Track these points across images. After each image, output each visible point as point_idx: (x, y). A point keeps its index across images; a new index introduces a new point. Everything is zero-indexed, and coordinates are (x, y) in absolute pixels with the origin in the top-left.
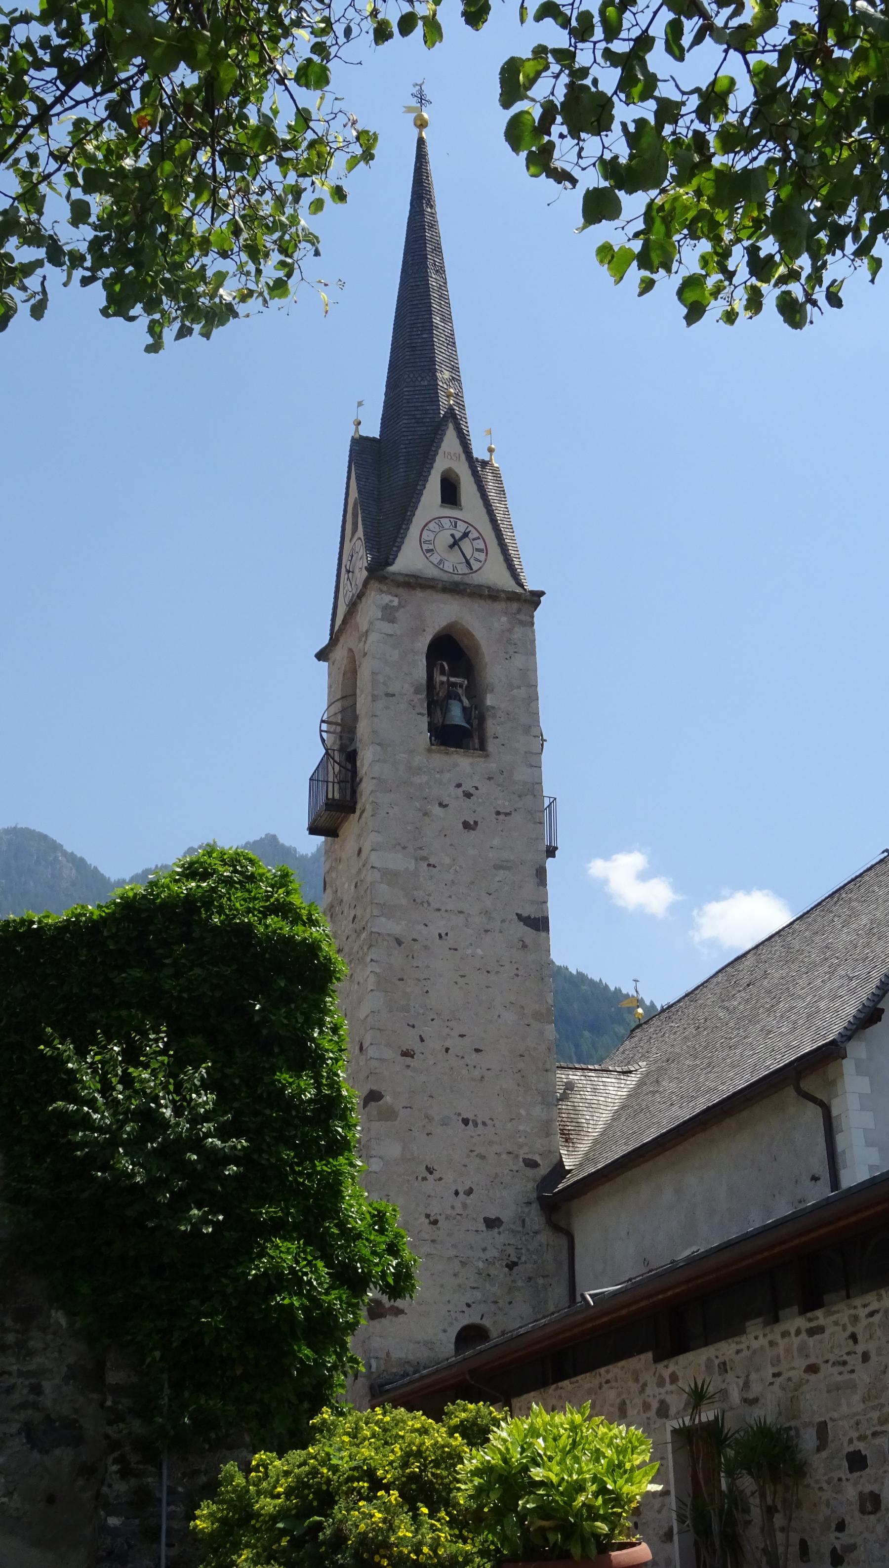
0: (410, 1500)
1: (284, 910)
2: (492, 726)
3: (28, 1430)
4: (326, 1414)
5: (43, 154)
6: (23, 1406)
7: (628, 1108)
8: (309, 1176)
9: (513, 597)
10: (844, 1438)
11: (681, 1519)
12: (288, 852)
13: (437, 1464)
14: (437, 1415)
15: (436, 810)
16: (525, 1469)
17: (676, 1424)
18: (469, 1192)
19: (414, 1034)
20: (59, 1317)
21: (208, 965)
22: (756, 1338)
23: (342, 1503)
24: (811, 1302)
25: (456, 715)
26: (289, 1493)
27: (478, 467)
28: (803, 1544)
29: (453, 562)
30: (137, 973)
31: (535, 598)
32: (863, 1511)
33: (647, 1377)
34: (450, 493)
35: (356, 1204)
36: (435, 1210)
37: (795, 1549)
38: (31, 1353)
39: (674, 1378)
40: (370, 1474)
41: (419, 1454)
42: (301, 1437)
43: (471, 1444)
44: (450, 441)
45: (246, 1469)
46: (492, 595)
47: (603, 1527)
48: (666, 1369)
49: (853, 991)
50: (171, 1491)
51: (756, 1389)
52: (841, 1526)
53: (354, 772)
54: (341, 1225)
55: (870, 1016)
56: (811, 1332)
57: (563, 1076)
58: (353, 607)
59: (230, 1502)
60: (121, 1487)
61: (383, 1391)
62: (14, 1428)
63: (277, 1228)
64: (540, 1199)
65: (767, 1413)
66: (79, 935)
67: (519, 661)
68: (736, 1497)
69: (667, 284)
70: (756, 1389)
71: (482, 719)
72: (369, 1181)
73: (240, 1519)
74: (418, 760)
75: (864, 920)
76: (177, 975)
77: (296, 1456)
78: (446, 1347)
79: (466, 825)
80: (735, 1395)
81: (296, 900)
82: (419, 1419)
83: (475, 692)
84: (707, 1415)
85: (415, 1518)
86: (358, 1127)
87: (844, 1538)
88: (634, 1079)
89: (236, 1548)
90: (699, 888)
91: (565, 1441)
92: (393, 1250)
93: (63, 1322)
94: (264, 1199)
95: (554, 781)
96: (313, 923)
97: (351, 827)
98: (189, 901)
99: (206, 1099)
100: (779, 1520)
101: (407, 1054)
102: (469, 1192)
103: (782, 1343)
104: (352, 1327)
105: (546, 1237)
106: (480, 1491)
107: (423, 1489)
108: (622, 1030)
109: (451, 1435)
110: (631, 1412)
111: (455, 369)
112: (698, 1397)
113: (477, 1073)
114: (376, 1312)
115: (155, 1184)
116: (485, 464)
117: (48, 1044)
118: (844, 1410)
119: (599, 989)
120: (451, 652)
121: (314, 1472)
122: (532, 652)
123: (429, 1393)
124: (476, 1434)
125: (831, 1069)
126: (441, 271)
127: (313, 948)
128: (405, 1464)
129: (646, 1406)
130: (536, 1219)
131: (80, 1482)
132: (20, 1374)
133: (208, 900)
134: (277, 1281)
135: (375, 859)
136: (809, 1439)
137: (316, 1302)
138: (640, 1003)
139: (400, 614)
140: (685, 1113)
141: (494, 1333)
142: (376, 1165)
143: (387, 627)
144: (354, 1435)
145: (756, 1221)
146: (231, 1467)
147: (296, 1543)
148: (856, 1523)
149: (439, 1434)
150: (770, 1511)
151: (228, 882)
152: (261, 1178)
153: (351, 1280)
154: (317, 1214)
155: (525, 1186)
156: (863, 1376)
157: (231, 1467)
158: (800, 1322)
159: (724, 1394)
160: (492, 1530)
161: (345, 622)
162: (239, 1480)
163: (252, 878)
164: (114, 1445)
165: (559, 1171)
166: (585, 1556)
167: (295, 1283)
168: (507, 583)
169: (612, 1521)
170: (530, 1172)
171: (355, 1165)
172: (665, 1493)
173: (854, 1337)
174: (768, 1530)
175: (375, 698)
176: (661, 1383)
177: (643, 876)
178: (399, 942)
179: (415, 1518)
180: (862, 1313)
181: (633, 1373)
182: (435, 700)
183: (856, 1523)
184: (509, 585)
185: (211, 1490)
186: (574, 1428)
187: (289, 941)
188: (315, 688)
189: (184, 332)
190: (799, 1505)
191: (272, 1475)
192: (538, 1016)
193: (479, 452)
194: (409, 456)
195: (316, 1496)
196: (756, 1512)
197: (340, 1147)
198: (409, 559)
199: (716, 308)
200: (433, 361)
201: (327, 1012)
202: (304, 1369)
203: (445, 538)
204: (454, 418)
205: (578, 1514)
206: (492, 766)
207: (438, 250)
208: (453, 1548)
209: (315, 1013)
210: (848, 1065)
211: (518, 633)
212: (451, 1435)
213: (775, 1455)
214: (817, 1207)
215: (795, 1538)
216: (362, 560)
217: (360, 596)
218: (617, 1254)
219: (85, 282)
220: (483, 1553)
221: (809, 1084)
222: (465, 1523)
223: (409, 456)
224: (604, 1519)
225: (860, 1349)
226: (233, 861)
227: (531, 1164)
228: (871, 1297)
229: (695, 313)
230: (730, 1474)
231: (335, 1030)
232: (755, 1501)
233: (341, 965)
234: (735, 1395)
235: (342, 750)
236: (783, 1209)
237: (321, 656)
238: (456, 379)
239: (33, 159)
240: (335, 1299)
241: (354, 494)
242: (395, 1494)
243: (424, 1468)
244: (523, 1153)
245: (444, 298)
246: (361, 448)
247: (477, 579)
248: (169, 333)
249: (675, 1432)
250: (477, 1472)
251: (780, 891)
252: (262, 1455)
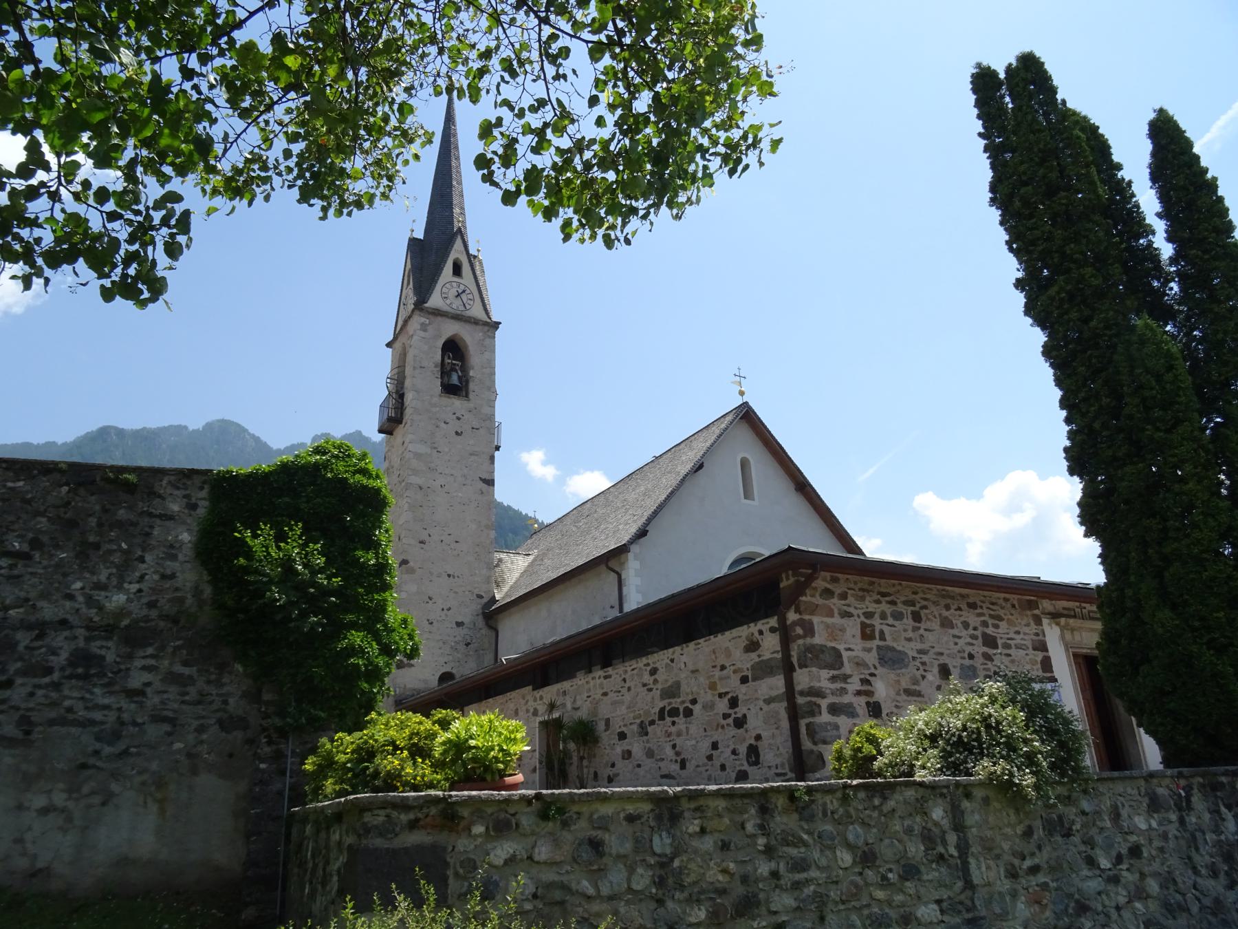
0: (413, 756)
1: (364, 472)
2: (472, 386)
3: (220, 722)
4: (373, 715)
5: (272, 121)
6: (217, 711)
7: (527, 572)
8: (371, 601)
9: (485, 324)
10: (617, 726)
11: (540, 763)
12: (367, 440)
13: (426, 738)
14: (427, 715)
15: (443, 425)
16: (467, 740)
17: (541, 719)
18: (449, 609)
19: (426, 533)
20: (239, 668)
21: (325, 498)
22: (581, 680)
23: (379, 757)
24: (606, 664)
25: (454, 379)
26: (353, 752)
27: (471, 258)
28: (596, 774)
29: (457, 304)
30: (287, 499)
31: (496, 325)
32: (623, 758)
33: (529, 697)
34: (457, 270)
35: (393, 615)
36: (431, 618)
37: (592, 776)
38: (223, 685)
39: (541, 698)
40: (393, 743)
41: (418, 734)
42: (359, 726)
43: (443, 729)
44: (458, 244)
45: (332, 741)
46: (476, 322)
47: (501, 766)
48: (538, 694)
49: (635, 521)
50: (293, 752)
51: (579, 703)
52: (613, 765)
53: (403, 404)
54: (386, 625)
55: (642, 533)
56: (606, 677)
57: (498, 556)
58: (406, 322)
59: (323, 757)
60: (267, 749)
61: (401, 704)
62: (213, 721)
63: (354, 626)
64: (483, 613)
65: (583, 714)
66: (256, 480)
67: (487, 355)
68: (566, 752)
69: (557, 222)
70: (579, 703)
71: (467, 382)
72: (399, 603)
73: (328, 764)
74: (435, 400)
75: (642, 488)
76: (308, 502)
77: (357, 734)
78: (433, 682)
79: (457, 433)
80: (569, 706)
81: (370, 467)
82: (419, 717)
83: (465, 369)
84: (556, 715)
85: (415, 763)
86: (395, 578)
87: (615, 770)
88: (531, 558)
89: (326, 778)
90: (568, 466)
91: (486, 728)
92: (411, 637)
93: (241, 669)
94: (347, 611)
95: (502, 412)
96: (378, 477)
97: (400, 431)
98: (316, 464)
99: (321, 561)
100: (585, 763)
101: (422, 542)
102: (449, 609)
103: (592, 683)
104: (388, 673)
105: (485, 631)
106: (445, 753)
107: (418, 751)
108: (527, 534)
109: (434, 724)
110: (521, 713)
111: (462, 208)
112: (552, 707)
113: (455, 553)
114: (400, 666)
115: (290, 603)
116: (475, 257)
117: (239, 532)
118: (618, 713)
119: (518, 514)
120: (453, 348)
121: (366, 742)
122: (493, 351)
123: (423, 705)
124: (445, 724)
125: (623, 556)
126: (458, 158)
127: (378, 491)
128: (411, 739)
129: (528, 711)
130: (481, 622)
131: (247, 747)
132: (217, 695)
133: (326, 465)
134: (353, 651)
135: (411, 447)
136: (601, 726)
137: (371, 663)
138: (536, 521)
139: (429, 328)
140: (554, 575)
141: (457, 676)
142: (404, 595)
143: (422, 334)
144: (386, 725)
145: (584, 626)
146: (324, 740)
147: (355, 776)
148: (620, 764)
149: (428, 724)
150: (582, 758)
151: (337, 457)
152: (348, 600)
153: (387, 651)
154: (373, 619)
155: (476, 606)
156: (628, 697)
157: (324, 740)
158: (601, 673)
159: (564, 705)
160: (450, 769)
161: (401, 329)
162: (328, 746)
163: (349, 456)
164: (264, 729)
165: (493, 600)
166: (493, 780)
167: (360, 652)
168: (483, 317)
169: (506, 763)
170: (479, 600)
171: (392, 596)
172: (533, 751)
173: (624, 680)
174: (580, 767)
175: (414, 368)
176: (535, 700)
177: (545, 463)
178: (421, 488)
179: (415, 763)
180: (629, 669)
181: (525, 697)
182: (445, 372)
183: (620, 764)
184: (485, 318)
185: (313, 750)
186: (490, 721)
187: (365, 487)
188: (384, 362)
189: (339, 213)
190: (595, 756)
191: (344, 745)
192: (487, 527)
193: (472, 251)
194: (436, 250)
195: (367, 754)
196: (575, 759)
197: (386, 587)
198: (435, 301)
199: (576, 236)
200: (451, 204)
201: (383, 522)
202: (363, 692)
203: (453, 292)
204: (461, 233)
205: (490, 761)
206: (471, 405)
207: (457, 148)
208: (431, 777)
209: (378, 523)
210: (631, 555)
211: (487, 341)
212: (434, 724)
213: (585, 733)
214: (611, 621)
215: (592, 771)
216: (411, 299)
217: (410, 317)
218: (519, 640)
219: (290, 187)
220: (446, 779)
221: (612, 564)
222: (438, 766)
223: (436, 250)
224: (502, 762)
225: (627, 685)
226: (339, 447)
227: (480, 597)
228: (634, 662)
229: (567, 237)
230: (564, 742)
231: (387, 531)
232: (575, 754)
233: (391, 499)
234: (569, 706)
235: (397, 392)
236: (597, 621)
237: (389, 345)
238: (463, 214)
239: (267, 123)
240: (381, 661)
241: (409, 266)
242: (406, 753)
243: (420, 740)
244: (476, 591)
245: (459, 172)
246: (413, 243)
247: (468, 313)
248: (331, 212)
249: (540, 723)
250: (444, 743)
251: (607, 475)
252: (340, 734)
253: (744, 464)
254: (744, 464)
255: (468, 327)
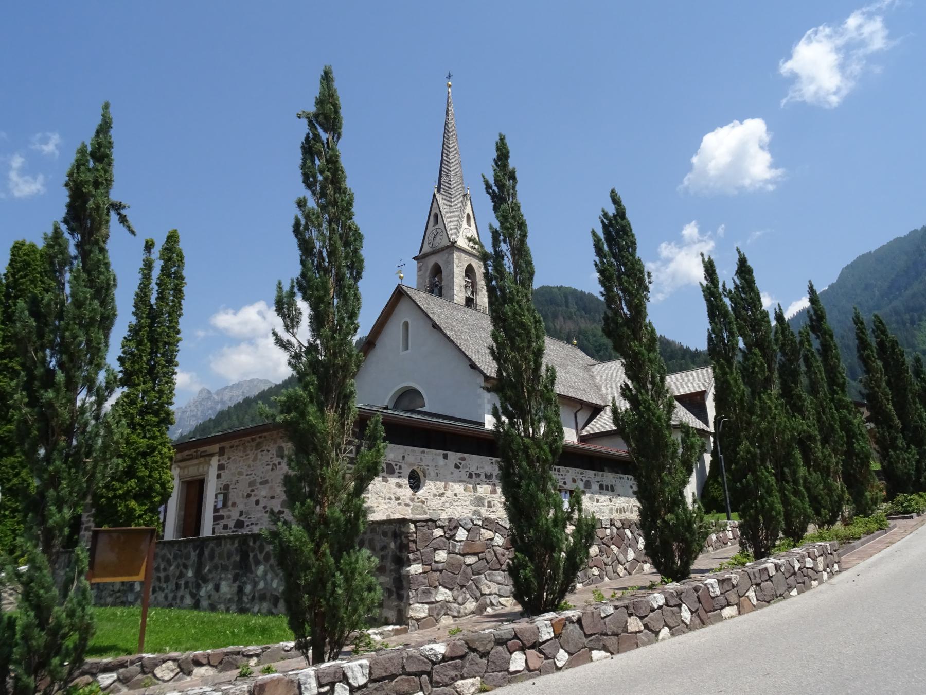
9: (447, 247)
34: (436, 222)
46: (442, 250)
253: (406, 325)
254: (406, 325)
255: (440, 255)
